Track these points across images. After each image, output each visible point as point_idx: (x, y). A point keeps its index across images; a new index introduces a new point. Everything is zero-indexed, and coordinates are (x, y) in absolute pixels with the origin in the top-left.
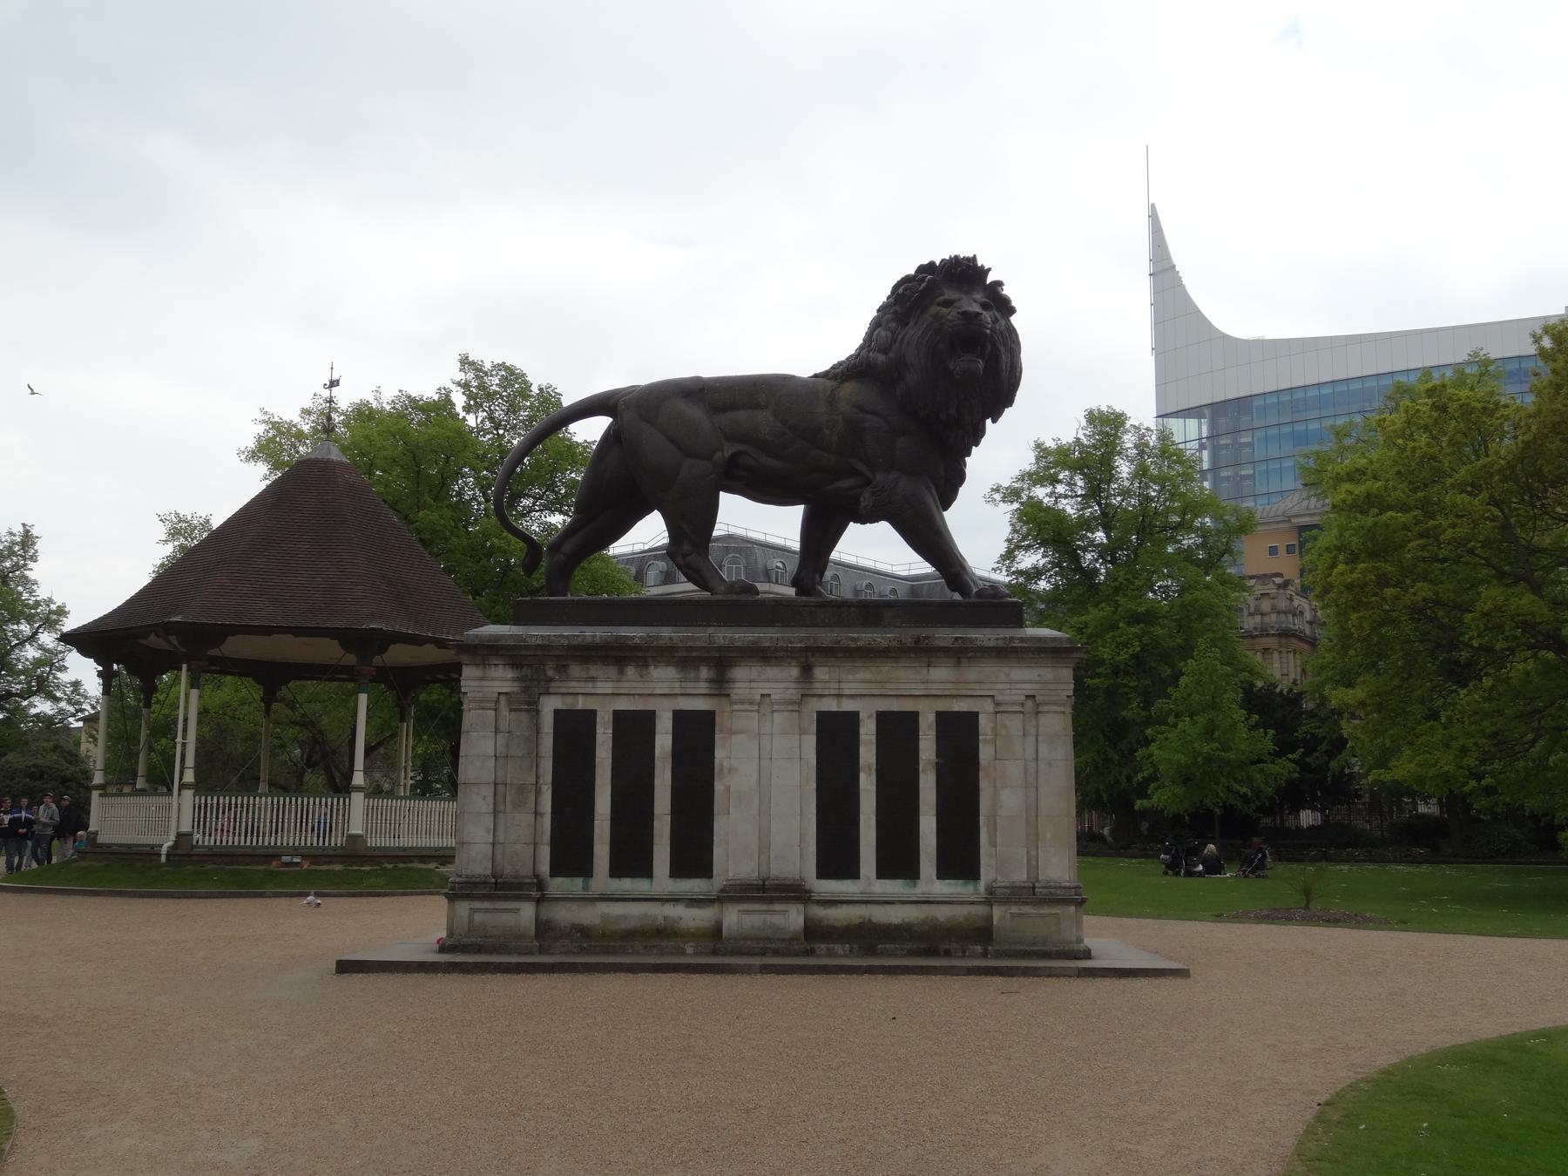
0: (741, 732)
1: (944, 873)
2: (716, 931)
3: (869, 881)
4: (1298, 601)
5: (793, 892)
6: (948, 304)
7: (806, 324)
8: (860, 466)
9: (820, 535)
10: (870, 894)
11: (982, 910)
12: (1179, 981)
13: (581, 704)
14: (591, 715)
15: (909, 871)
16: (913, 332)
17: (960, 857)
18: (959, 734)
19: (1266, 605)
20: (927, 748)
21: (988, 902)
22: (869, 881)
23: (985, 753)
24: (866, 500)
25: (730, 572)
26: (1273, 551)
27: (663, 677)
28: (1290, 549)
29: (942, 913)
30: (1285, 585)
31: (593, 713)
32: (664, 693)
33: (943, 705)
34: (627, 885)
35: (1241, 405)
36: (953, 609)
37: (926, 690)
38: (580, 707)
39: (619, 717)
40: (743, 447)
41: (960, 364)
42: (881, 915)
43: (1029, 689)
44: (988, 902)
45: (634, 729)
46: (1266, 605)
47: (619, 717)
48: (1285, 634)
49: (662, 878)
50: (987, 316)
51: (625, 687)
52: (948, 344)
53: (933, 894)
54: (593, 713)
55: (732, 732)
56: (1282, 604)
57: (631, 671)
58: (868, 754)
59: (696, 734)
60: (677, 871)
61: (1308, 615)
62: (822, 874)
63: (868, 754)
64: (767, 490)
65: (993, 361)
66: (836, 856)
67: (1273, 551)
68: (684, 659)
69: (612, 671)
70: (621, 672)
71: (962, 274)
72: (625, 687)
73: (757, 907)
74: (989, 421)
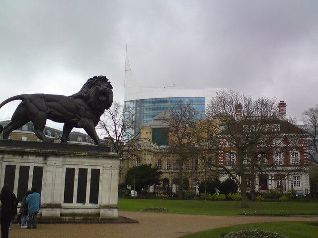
0: (49, 171)
1: (91, 202)
2: (98, 214)
3: (75, 203)
4: (152, 144)
5: (58, 206)
6: (100, 85)
7: (66, 83)
8: (78, 116)
9: (67, 129)
10: (75, 207)
11: (98, 210)
12: (137, 224)
13: (12, 164)
14: (14, 167)
15: (84, 202)
16: (92, 90)
17: (94, 199)
18: (96, 173)
19: (145, 144)
20: (89, 177)
21: (99, 208)
22: (75, 203)
23: (101, 177)
24: (79, 123)
25: (49, 137)
26: (147, 133)
27: (32, 158)
28: (150, 133)
29: (90, 211)
30: (150, 140)
31: (29, 167)
32: (32, 162)
33: (93, 168)
34: (80, 205)
35: (142, 101)
36: (102, 149)
37: (89, 164)
38: (12, 164)
39: (21, 167)
40: (51, 110)
41: (103, 98)
42: (76, 211)
43: (110, 165)
44: (99, 208)
45: (24, 170)
46: (145, 144)
47: (21, 167)
48: (149, 151)
49: (88, 204)
50: (108, 89)
51: (23, 161)
52: (98, 94)
53: (88, 207)
54: (29, 167)
55: (47, 171)
56: (149, 144)
57: (25, 157)
58: (76, 177)
59: (39, 171)
60: (91, 202)
61: (153, 147)
62: (65, 202)
63: (76, 177)
64: (56, 119)
65: (108, 97)
66: (68, 198)
67: (147, 133)
68: (38, 155)
69: (20, 157)
70: (22, 157)
71: (103, 79)
72: (23, 161)
73: (50, 209)
74: (106, 110)
